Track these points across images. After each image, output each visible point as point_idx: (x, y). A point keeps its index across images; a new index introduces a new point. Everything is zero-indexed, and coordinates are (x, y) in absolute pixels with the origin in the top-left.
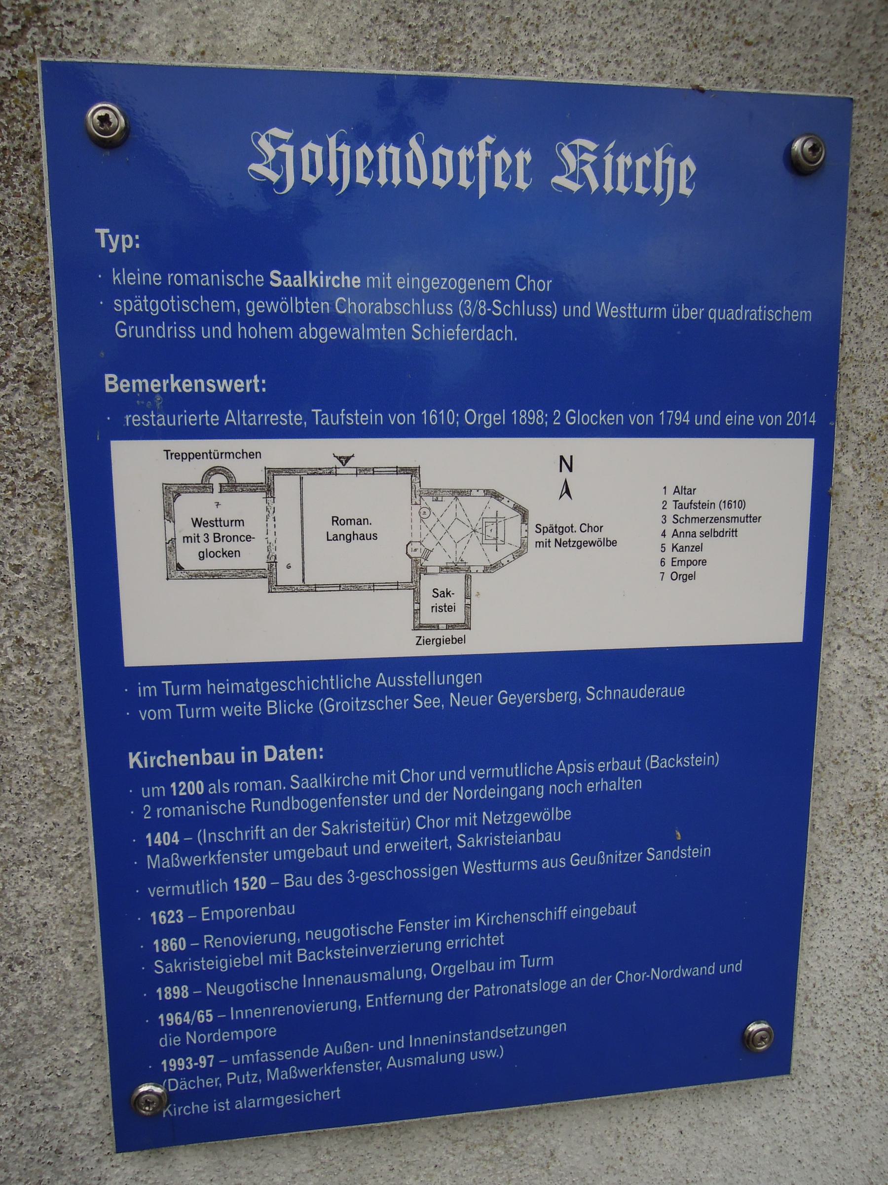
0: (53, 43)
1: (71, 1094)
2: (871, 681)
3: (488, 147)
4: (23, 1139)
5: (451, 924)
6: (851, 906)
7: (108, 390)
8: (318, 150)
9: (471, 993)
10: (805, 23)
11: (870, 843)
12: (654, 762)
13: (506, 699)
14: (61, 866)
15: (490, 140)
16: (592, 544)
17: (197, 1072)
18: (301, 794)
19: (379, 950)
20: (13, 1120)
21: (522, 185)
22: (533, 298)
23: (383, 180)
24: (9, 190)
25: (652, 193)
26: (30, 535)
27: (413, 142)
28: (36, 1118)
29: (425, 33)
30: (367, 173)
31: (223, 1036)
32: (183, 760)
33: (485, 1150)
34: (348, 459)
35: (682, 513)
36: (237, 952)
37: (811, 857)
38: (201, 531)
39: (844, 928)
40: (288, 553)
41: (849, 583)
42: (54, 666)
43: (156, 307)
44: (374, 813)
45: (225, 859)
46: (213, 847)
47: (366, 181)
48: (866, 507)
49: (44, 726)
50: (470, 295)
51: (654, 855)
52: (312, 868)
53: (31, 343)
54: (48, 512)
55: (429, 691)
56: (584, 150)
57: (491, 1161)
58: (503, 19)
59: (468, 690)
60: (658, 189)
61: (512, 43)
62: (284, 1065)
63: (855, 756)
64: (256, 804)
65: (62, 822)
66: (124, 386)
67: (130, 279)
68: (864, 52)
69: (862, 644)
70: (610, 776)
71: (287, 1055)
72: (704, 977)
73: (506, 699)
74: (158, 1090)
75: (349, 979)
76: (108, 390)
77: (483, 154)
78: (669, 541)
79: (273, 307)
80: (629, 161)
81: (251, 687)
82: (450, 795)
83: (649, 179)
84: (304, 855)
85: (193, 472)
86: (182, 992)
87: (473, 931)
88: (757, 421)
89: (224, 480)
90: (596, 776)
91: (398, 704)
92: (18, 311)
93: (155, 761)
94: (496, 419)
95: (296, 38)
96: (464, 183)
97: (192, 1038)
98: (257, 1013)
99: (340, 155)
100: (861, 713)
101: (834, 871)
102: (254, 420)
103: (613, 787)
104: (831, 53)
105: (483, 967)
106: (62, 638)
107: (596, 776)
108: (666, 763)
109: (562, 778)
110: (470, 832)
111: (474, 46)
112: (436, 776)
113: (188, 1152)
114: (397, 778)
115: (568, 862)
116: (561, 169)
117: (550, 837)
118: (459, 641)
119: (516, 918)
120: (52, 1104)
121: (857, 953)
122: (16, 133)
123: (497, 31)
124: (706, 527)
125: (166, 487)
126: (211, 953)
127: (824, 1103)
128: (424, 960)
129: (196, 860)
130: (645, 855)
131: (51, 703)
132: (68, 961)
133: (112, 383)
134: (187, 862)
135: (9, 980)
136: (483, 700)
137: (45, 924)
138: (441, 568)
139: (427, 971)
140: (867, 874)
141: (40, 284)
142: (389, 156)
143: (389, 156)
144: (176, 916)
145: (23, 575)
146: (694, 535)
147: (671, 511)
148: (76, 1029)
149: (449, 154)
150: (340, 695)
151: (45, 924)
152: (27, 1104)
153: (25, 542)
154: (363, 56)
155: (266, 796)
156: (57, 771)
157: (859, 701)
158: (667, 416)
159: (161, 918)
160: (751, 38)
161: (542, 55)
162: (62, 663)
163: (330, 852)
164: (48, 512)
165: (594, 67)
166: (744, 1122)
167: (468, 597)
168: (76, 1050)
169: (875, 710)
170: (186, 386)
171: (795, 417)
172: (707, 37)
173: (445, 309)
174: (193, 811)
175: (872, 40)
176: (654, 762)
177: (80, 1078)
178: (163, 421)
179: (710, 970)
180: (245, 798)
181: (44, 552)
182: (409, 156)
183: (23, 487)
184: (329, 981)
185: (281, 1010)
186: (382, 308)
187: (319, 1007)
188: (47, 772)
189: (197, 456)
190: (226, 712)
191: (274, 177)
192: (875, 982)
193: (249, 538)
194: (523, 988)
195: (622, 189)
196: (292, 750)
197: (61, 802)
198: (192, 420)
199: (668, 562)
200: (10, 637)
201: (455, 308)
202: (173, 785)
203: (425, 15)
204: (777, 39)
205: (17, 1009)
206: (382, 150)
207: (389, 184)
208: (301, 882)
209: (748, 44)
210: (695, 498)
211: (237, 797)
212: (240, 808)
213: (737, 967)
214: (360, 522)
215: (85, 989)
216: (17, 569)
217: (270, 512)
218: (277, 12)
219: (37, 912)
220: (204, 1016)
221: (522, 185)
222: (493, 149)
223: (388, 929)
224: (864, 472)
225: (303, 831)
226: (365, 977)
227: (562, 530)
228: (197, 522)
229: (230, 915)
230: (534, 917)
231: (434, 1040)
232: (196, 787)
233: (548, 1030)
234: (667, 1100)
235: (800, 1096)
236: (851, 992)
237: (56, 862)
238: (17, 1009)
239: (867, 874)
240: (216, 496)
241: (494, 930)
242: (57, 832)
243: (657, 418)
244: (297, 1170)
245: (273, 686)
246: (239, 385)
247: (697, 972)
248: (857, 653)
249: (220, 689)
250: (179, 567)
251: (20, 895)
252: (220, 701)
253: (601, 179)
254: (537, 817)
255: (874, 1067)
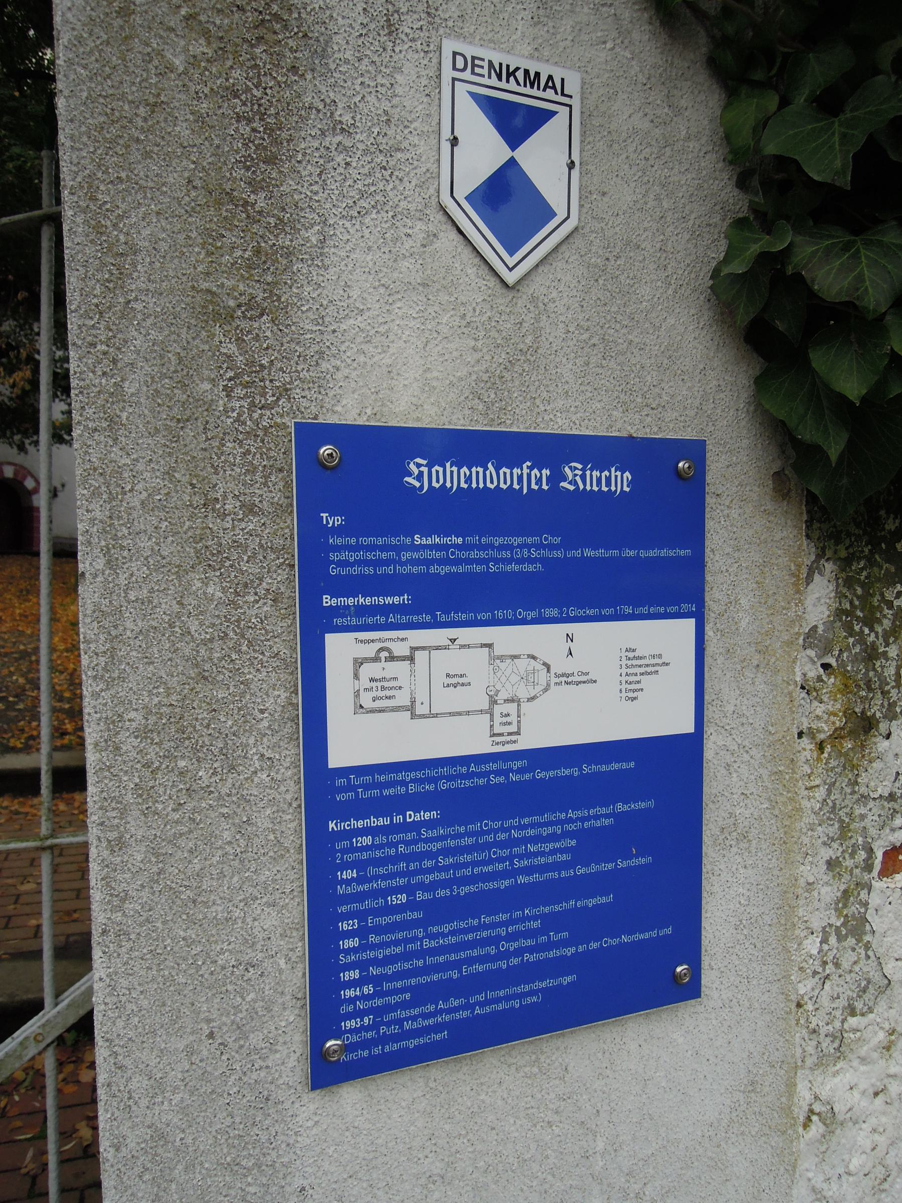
0: (294, 408)
1: (278, 1056)
2: (729, 753)
3: (528, 467)
4: (245, 1092)
5: (511, 916)
6: (727, 890)
7: (325, 605)
8: (441, 469)
9: (522, 960)
10: (680, 398)
11: (734, 850)
12: (620, 807)
13: (540, 775)
14: (280, 898)
15: (529, 464)
16: (584, 682)
17: (363, 1028)
18: (427, 840)
19: (470, 937)
20: (240, 1079)
21: (545, 487)
22: (552, 547)
23: (474, 485)
24: (266, 489)
25: (610, 490)
26: (271, 690)
27: (490, 465)
28: (254, 1076)
29: (493, 405)
30: (466, 482)
31: (379, 1002)
32: (360, 824)
33: (527, 1069)
34: (455, 640)
35: (629, 663)
36: (387, 945)
37: (705, 861)
38: (374, 684)
39: (723, 903)
40: (421, 696)
41: (714, 697)
42: (283, 770)
43: (353, 557)
44: (468, 849)
45: (383, 884)
46: (376, 877)
47: (466, 486)
48: (721, 653)
49: (275, 809)
50: (519, 546)
51: (622, 864)
52: (432, 887)
53: (275, 576)
54: (282, 676)
55: (498, 773)
56: (576, 468)
57: (530, 1077)
58: (532, 398)
59: (520, 771)
60: (613, 488)
61: (537, 410)
62: (414, 1018)
63: (724, 798)
64: (401, 849)
65: (282, 869)
66: (334, 602)
67: (339, 541)
68: (709, 412)
69: (723, 731)
70: (597, 817)
71: (416, 1011)
72: (651, 939)
73: (540, 775)
74: (339, 1042)
75: (453, 957)
76: (325, 605)
77: (526, 471)
78: (624, 679)
79: (416, 555)
80: (598, 474)
81: (400, 777)
82: (510, 835)
83: (608, 483)
84: (428, 879)
85: (370, 651)
86: (355, 974)
87: (524, 919)
88: (666, 610)
89: (387, 654)
90: (588, 818)
91: (482, 782)
92: (268, 558)
93: (345, 826)
94: (532, 614)
95: (425, 407)
96: (516, 486)
97: (360, 1005)
98: (399, 984)
99: (452, 472)
100: (724, 772)
101: (716, 868)
102: (404, 619)
103: (598, 824)
104: (692, 413)
105: (529, 942)
106: (288, 753)
107: (588, 818)
108: (626, 808)
109: (570, 821)
110: (521, 857)
111: (517, 411)
112: (502, 824)
113: (350, 1089)
114: (481, 826)
115: (575, 872)
116: (564, 479)
117: (565, 857)
118: (515, 742)
119: (547, 910)
120: (265, 1064)
121: (732, 919)
122: (271, 457)
123: (528, 404)
124: (642, 670)
125: (355, 660)
126: (373, 947)
127: (720, 1019)
128: (494, 941)
129: (366, 887)
130: (617, 864)
131: (280, 794)
132: (282, 962)
133: (327, 601)
134: (361, 888)
135: (245, 978)
136: (527, 776)
137: (269, 938)
138: (505, 701)
139: (497, 948)
140: (734, 869)
141: (281, 542)
142: (477, 473)
143: (477, 473)
144: (354, 924)
145: (266, 715)
146: (636, 675)
147: (624, 662)
148: (285, 1009)
149: (508, 471)
150: (450, 778)
151: (269, 938)
152: (250, 1066)
153: (268, 695)
154: (460, 417)
155: (407, 843)
156: (281, 837)
157: (724, 765)
158: (621, 609)
159: (344, 926)
160: (654, 406)
161: (551, 416)
162: (288, 768)
163: (443, 876)
164: (282, 676)
165: (577, 422)
166: (675, 1036)
167: (519, 716)
168: (283, 1024)
169: (732, 769)
170: (368, 601)
171: (685, 607)
172: (632, 406)
173: (506, 554)
174: (365, 856)
175: (713, 405)
176: (620, 807)
177: (285, 1043)
178: (354, 621)
179: (654, 934)
180: (395, 845)
181: (279, 700)
182: (488, 473)
183: (267, 662)
184: (441, 959)
185: (413, 981)
186: (475, 554)
187: (435, 977)
188: (276, 838)
189: (373, 641)
190: (386, 792)
191: (417, 484)
192: (743, 937)
193: (400, 688)
194: (551, 954)
195: (595, 488)
196: (422, 813)
197: (282, 856)
198: (370, 620)
199: (624, 690)
200: (257, 754)
201: (512, 553)
202: (354, 840)
203: (493, 396)
204: (667, 406)
205: (249, 998)
206: (474, 470)
207: (478, 487)
208: (427, 896)
209: (652, 409)
210: (636, 654)
211: (391, 845)
212: (392, 852)
213: (669, 931)
214: (461, 676)
215: (291, 981)
216: (262, 711)
217: (412, 672)
218: (416, 394)
219: (265, 930)
220: (368, 989)
221: (545, 487)
222: (531, 468)
223: (475, 922)
224: (719, 634)
225: (428, 864)
226: (462, 955)
227: (568, 676)
228: (372, 680)
229: (385, 920)
230: (557, 908)
231: (501, 993)
232: (367, 840)
233: (567, 980)
234: (631, 1024)
235: (706, 1015)
236: (729, 945)
237: (278, 896)
238: (249, 998)
239: (734, 869)
240: (383, 664)
241: (535, 918)
242: (279, 876)
243: (616, 610)
244: (415, 1096)
245: (412, 775)
246: (396, 600)
247: (647, 936)
248: (721, 737)
249: (382, 778)
250: (361, 707)
251: (255, 920)
252: (382, 786)
253: (585, 484)
254: (557, 845)
255: (746, 992)
